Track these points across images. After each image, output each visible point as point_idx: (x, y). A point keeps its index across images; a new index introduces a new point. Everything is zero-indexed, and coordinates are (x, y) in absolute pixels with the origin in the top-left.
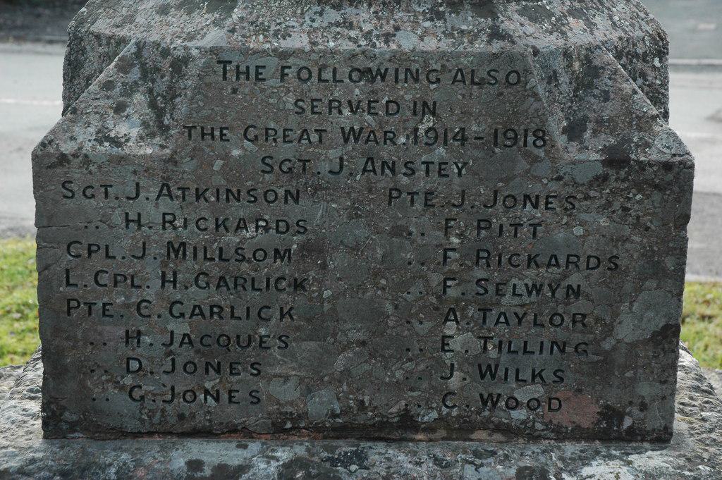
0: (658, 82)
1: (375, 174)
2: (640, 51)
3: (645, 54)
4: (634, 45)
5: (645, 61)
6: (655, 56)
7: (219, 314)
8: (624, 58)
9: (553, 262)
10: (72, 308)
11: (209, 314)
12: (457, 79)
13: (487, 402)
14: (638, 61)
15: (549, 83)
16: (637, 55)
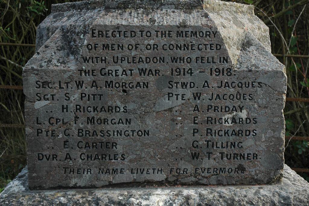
0: (80, 45)
1: (123, 124)
2: (77, 31)
3: (78, 33)
4: (75, 28)
5: (78, 35)
6: (82, 33)
7: (241, 134)
8: (69, 33)
9: (121, 121)
10: (196, 132)
11: (118, 122)
12: (102, 110)
13: (196, 97)
14: (74, 35)
15: (40, 39)
16: (75, 32)
